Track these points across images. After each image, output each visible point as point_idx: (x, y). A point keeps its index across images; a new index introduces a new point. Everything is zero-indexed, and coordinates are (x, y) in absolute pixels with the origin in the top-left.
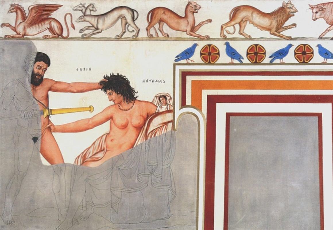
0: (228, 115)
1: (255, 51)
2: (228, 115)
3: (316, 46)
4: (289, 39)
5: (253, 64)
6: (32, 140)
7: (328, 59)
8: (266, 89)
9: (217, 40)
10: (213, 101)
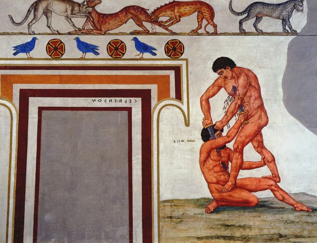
0: (41, 109)
1: (57, 46)
2: (41, 109)
3: (74, 39)
4: (32, 34)
5: (114, 59)
6: (224, 131)
7: (87, 53)
8: (49, 82)
9: (115, 34)
10: (25, 95)
